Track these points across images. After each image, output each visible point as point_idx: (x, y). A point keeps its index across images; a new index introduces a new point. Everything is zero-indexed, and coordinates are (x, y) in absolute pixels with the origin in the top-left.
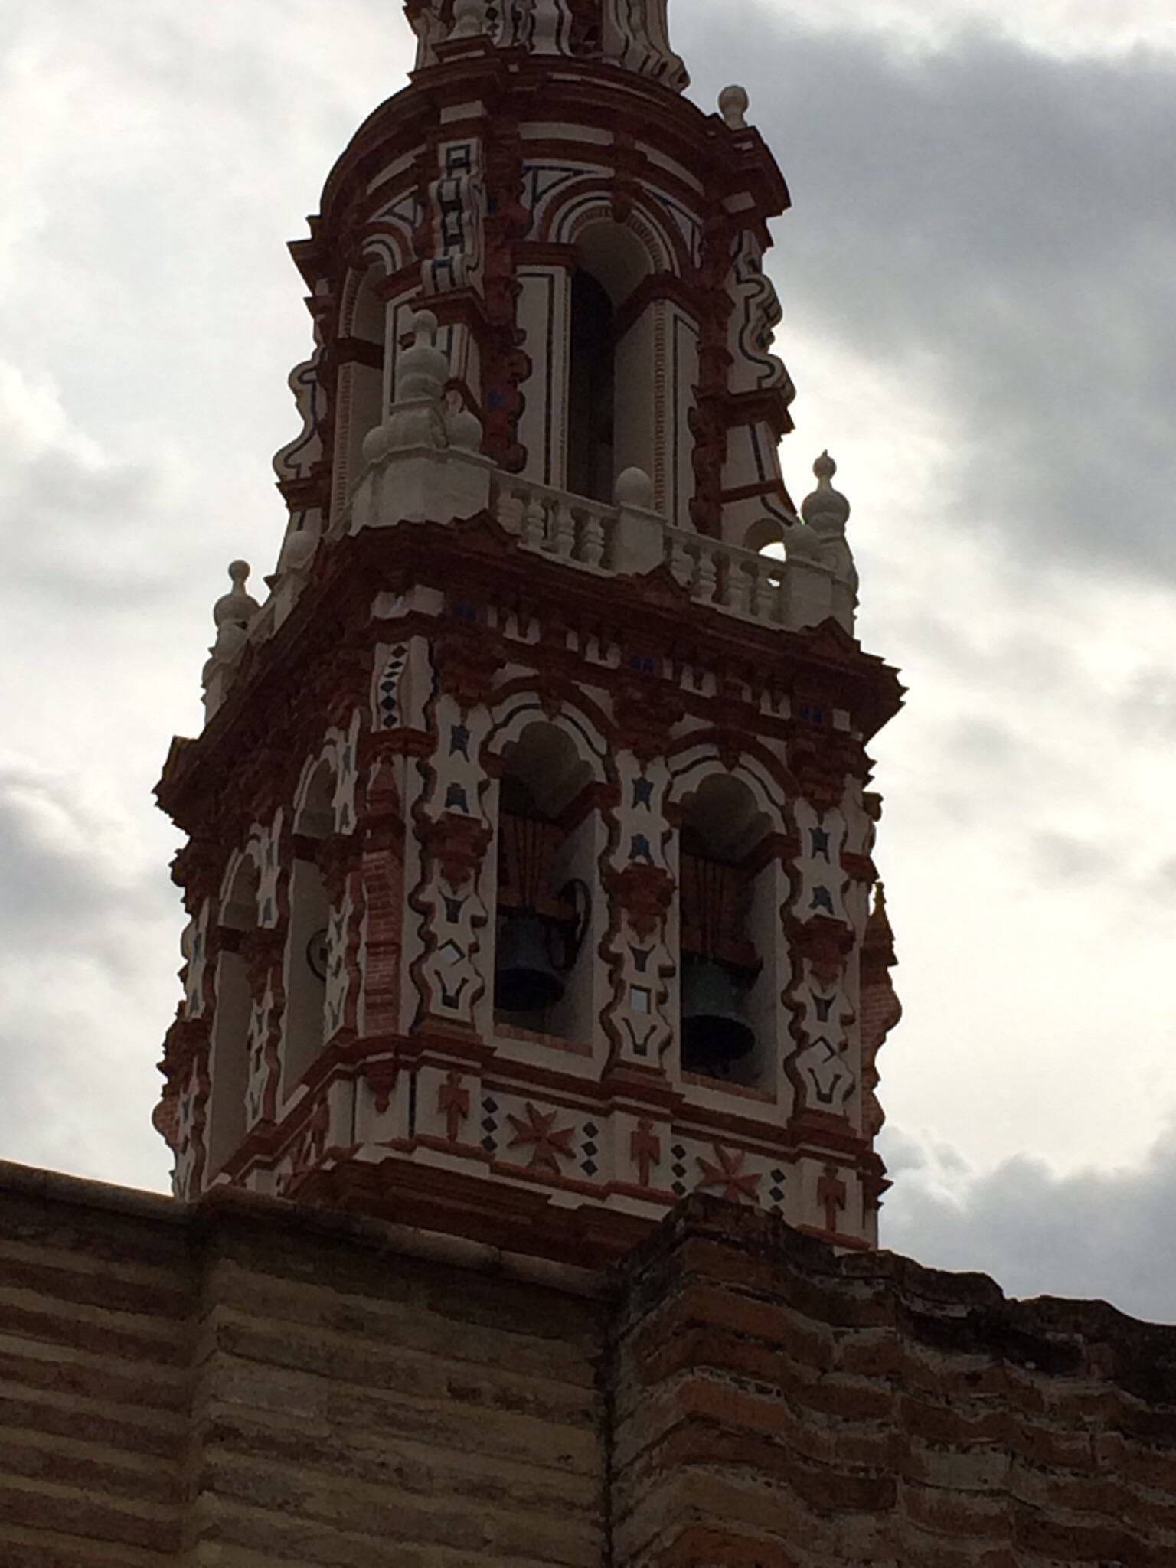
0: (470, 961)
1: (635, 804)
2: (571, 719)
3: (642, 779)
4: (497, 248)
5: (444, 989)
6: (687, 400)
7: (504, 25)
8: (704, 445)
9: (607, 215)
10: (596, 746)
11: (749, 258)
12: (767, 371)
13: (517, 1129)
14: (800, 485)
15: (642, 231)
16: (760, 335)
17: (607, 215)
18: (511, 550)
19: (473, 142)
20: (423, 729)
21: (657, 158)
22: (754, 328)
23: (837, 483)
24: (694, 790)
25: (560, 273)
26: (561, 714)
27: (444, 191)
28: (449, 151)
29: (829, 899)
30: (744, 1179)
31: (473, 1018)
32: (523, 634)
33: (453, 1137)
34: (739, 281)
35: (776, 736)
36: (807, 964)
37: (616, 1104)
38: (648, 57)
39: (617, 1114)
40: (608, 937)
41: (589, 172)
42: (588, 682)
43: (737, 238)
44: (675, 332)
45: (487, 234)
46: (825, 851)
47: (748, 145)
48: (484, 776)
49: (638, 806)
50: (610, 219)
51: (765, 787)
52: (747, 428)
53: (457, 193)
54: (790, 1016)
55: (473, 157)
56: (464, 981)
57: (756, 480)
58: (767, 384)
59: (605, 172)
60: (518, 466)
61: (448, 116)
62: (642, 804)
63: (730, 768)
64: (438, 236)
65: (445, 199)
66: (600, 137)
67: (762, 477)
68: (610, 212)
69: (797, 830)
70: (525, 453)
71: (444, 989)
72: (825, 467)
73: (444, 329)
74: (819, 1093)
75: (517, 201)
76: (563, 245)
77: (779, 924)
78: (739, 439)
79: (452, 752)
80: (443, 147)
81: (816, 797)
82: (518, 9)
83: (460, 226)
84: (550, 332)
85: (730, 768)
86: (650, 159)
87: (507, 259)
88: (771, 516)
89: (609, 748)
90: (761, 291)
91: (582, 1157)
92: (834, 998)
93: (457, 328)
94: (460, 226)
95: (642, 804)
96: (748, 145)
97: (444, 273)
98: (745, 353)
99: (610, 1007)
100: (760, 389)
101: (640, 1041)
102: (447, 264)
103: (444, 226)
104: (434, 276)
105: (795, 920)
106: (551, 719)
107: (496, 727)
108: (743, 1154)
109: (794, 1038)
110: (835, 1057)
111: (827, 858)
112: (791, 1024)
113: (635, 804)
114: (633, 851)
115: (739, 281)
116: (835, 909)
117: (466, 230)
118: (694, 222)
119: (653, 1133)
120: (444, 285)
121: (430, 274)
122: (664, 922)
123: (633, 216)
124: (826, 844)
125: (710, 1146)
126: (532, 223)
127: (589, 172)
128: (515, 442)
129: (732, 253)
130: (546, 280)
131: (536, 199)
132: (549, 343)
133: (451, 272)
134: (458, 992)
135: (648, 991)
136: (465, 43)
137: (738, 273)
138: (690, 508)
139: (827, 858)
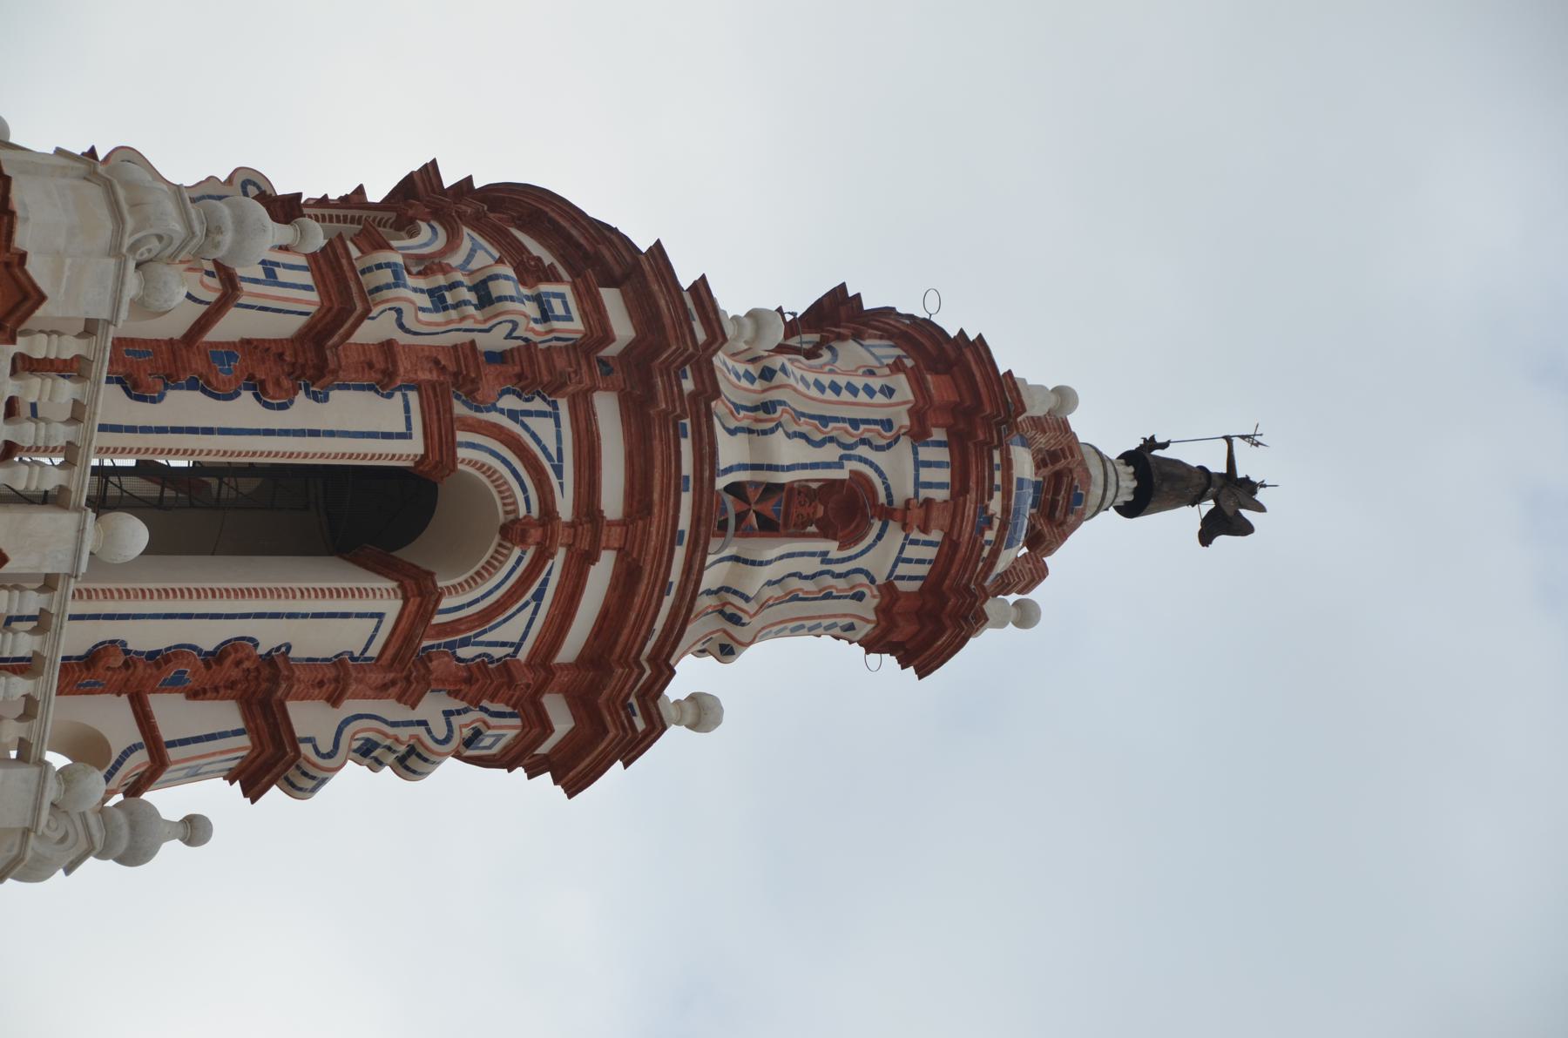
4: (437, 362)
6: (268, 636)
7: (754, 391)
8: (208, 665)
9: (507, 513)
11: (483, 728)
12: (325, 749)
14: (168, 801)
15: (491, 568)
16: (376, 745)
17: (507, 513)
19: (577, 325)
21: (600, 576)
22: (386, 736)
23: (172, 850)
25: (415, 447)
27: (502, 282)
28: (561, 296)
34: (448, 714)
38: (747, 599)
41: (561, 485)
43: (509, 710)
44: (359, 615)
45: (455, 347)
47: (640, 724)
50: (502, 518)
52: (240, 725)
53: (501, 299)
55: (556, 325)
57: (166, 737)
58: (306, 749)
59: (565, 507)
60: (135, 389)
61: (611, 298)
64: (440, 280)
65: (491, 284)
66: (612, 501)
67: (172, 744)
68: (511, 517)
70: (153, 401)
72: (194, 830)
73: (302, 261)
75: (507, 391)
76: (454, 453)
78: (225, 714)
80: (566, 289)
82: (779, 409)
83: (456, 306)
84: (331, 434)
86: (593, 570)
87: (424, 376)
88: (115, 756)
90: (437, 741)
93: (314, 296)
94: (456, 306)
96: (640, 724)
97: (386, 276)
98: (347, 722)
100: (295, 742)
102: (398, 283)
103: (453, 286)
104: (379, 267)
115: (448, 714)
117: (453, 314)
118: (518, 646)
120: (370, 281)
121: (383, 261)
123: (511, 550)
126: (478, 409)
127: (561, 485)
128: (167, 387)
129: (485, 703)
130: (402, 429)
131: (513, 415)
132: (314, 433)
133: (388, 287)
136: (712, 315)
137: (459, 712)
138: (113, 642)
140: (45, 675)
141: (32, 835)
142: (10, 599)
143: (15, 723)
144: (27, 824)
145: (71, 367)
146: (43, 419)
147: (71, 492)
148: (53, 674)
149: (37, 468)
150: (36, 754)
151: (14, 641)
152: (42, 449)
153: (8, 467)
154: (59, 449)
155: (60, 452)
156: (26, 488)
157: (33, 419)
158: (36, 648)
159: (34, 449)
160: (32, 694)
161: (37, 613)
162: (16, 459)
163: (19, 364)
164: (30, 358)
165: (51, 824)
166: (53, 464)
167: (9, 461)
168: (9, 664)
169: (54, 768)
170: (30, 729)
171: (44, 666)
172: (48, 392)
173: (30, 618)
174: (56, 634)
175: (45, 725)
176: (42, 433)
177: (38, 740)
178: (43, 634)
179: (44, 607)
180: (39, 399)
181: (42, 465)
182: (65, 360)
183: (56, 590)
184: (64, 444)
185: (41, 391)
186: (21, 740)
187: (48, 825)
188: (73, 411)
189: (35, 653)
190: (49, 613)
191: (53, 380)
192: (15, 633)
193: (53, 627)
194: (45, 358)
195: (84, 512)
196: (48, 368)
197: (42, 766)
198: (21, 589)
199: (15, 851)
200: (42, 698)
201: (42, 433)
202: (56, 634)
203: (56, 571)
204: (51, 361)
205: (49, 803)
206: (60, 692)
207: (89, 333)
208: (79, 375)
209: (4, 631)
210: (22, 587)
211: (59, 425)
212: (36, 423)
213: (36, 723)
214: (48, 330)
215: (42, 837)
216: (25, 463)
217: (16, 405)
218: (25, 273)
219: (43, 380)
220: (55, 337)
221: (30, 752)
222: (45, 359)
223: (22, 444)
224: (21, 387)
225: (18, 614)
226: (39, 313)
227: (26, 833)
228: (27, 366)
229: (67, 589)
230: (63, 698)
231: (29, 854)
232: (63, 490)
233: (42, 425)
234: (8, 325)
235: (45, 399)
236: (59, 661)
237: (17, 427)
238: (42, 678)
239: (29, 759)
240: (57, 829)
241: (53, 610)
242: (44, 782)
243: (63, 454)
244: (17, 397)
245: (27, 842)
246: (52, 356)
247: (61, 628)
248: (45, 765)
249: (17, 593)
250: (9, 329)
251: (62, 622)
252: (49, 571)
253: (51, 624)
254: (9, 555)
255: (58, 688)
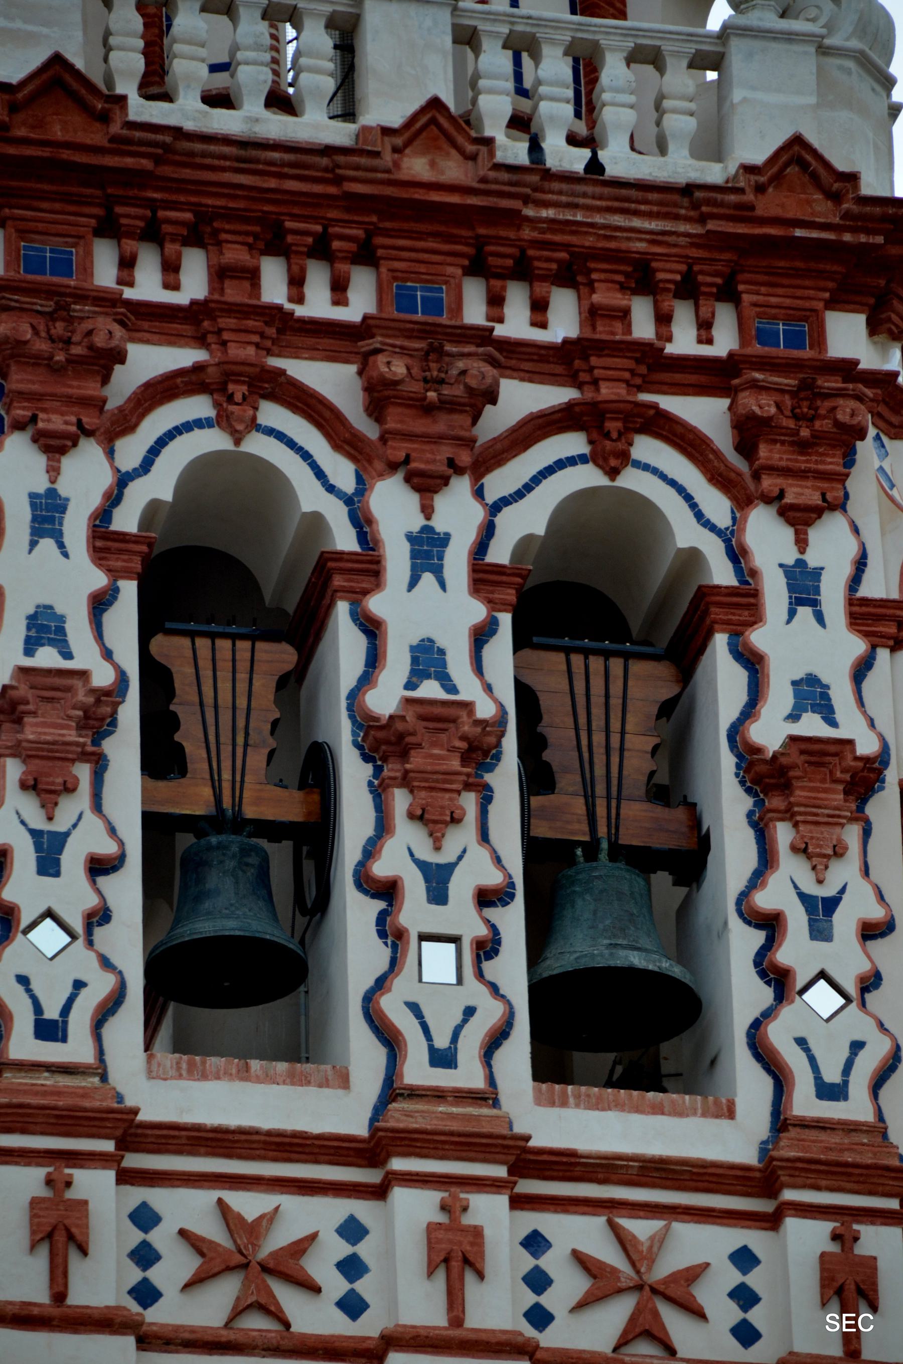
0: (90, 943)
1: (413, 582)
2: (280, 436)
3: (427, 529)
5: (38, 1008)
10: (709, 513)
13: (202, 1254)
18: (115, 128)
20: (735, 583)
24: (540, 530)
26: (258, 428)
29: (825, 696)
30: (275, 1254)
31: (491, 1080)
32: (172, 285)
33: (456, 1318)
35: (333, 357)
36: (783, 834)
37: (394, 1173)
39: (791, 1223)
40: (371, 851)
42: (295, 353)
46: (814, 603)
48: (99, 579)
49: (421, 583)
51: (688, 498)
54: (758, 938)
56: (79, 985)
62: (428, 579)
63: (613, 473)
69: (754, 573)
71: (38, 1008)
74: (432, 1050)
77: (728, 761)
79: (33, 544)
81: (789, 499)
85: (613, 473)
89: (360, 480)
91: (732, 1314)
92: (843, 890)
95: (428, 579)
99: (381, 984)
101: (442, 1041)
105: (757, 750)
106: (237, 442)
107: (123, 481)
108: (667, 1228)
109: (768, 983)
110: (853, 1006)
111: (820, 618)
112: (382, 919)
113: (413, 582)
114: (413, 672)
116: (839, 716)
119: (73, 1194)
122: (867, 833)
124: (817, 591)
125: (600, 1221)
134: (66, 1009)
135: (455, 940)
139: (820, 618)
140: (597, 37)
141: (827, 42)
142: (491, 91)
143: (667, 77)
144: (812, 49)
145: (155, 15)
146: (232, 54)
147: (334, 11)
148: (595, 26)
149: (303, 61)
150: (710, 43)
151: (551, 84)
152: (275, 54)
153: (303, 101)
154: (273, 31)
155: (277, 30)
156: (331, 75)
157: (232, 68)
158: (559, 51)
159: (275, 66)
160: (625, 54)
161: (510, 53)
162: (291, 90)
163: (154, 90)
164: (146, 75)
165: (812, 16)
166: (296, 38)
167: (293, 100)
168: (583, 89)
169: (730, 17)
170: (676, 54)
171: (586, 39)
172: (194, 48)
173: (517, 62)
174: (538, 25)
175: (671, 33)
176: (251, 55)
177: (691, 41)
178: (539, 42)
179: (500, 43)
180: (203, 60)
181: (298, 54)
182: (145, 25)
183: (475, 28)
184: (266, 23)
185: (193, 58)
186: (691, 66)
187: (813, 20)
188: (218, 12)
189: (566, 53)
190: (509, 35)
191: (175, 41)
192: (538, 82)
193: (528, 29)
194: (143, 53)
195: (728, 31)
196: (157, 49)
197: (728, 34)
198: (476, 77)
199: (851, 64)
200: (630, 39)
201: (251, 55)
202: (538, 25)
203: (449, 29)
204: (147, 44)
205: (782, 20)
206: (622, 14)
207: (473, 34)
208: (165, 5)
209: (536, 97)
210: (473, 74)
211: (239, 30)
212: (239, 64)
213: (666, 47)
214: (102, 51)
215: (830, 27)
216: (295, 78)
217: (214, 92)
218: (23, 83)
219: (175, 56)
220: (112, 41)
221: (708, 52)
222: (145, 53)
223: (269, 83)
224: (188, 86)
225: (512, 79)
226: (79, 63)
227: (823, 50)
228: (157, 79)
229: (474, 11)
230: (629, 11)
231: (854, 44)
232: (331, 24)
233: (240, 56)
234: (100, 106)
235: (202, 52)
236: (577, 18)
237: (244, 91)
238: (601, 42)
239: (719, 53)
240: (817, 7)
241: (505, 30)
242: (751, 30)
243: (280, 25)
244: (203, 91)
245: (838, 49)
246: (141, 44)
247: (529, 18)
248: (727, 30)
249: (482, 83)
250: (106, 106)
251: (522, 17)
252: (448, 39)
253: (524, 33)
254: (428, 96)
255: (615, 18)
